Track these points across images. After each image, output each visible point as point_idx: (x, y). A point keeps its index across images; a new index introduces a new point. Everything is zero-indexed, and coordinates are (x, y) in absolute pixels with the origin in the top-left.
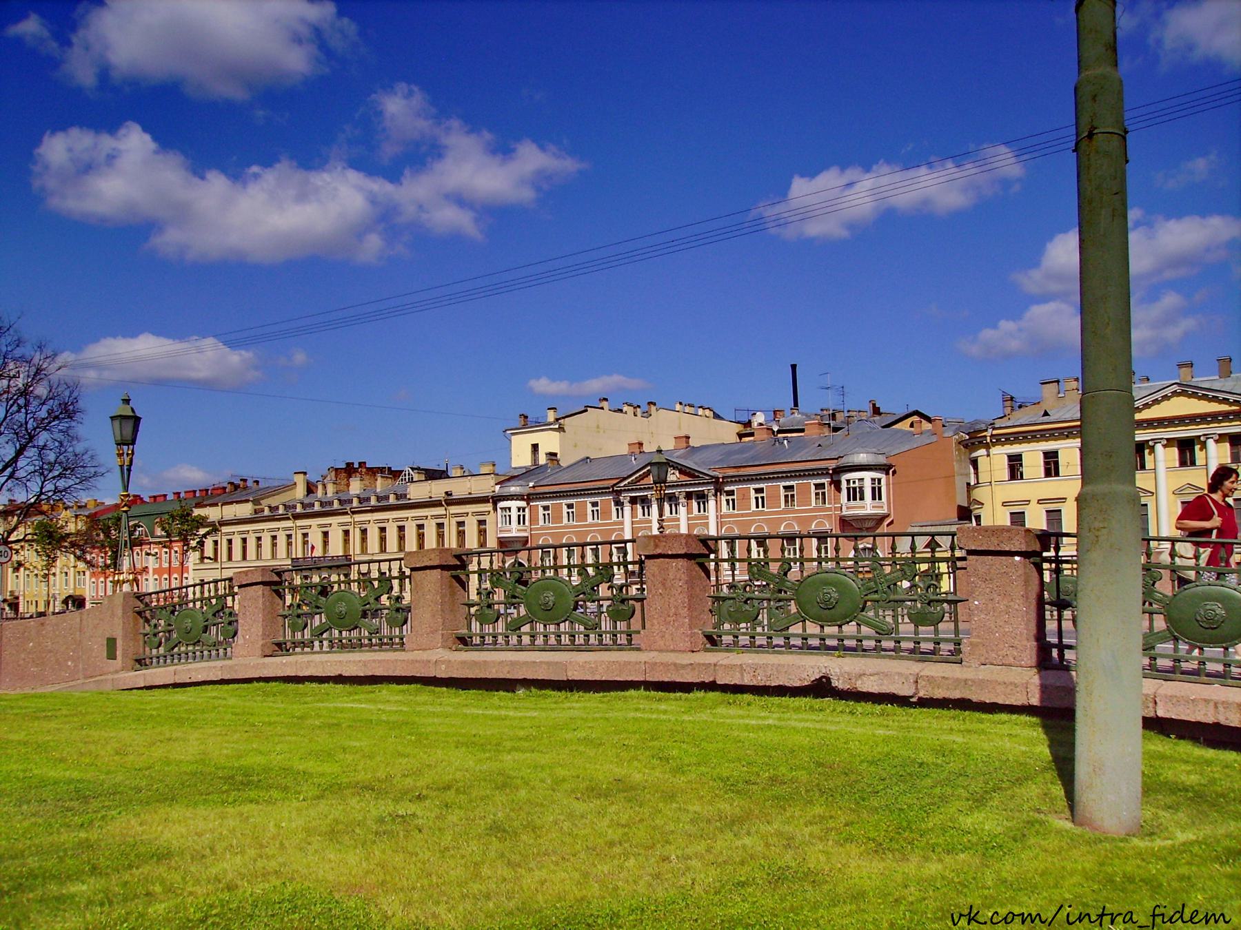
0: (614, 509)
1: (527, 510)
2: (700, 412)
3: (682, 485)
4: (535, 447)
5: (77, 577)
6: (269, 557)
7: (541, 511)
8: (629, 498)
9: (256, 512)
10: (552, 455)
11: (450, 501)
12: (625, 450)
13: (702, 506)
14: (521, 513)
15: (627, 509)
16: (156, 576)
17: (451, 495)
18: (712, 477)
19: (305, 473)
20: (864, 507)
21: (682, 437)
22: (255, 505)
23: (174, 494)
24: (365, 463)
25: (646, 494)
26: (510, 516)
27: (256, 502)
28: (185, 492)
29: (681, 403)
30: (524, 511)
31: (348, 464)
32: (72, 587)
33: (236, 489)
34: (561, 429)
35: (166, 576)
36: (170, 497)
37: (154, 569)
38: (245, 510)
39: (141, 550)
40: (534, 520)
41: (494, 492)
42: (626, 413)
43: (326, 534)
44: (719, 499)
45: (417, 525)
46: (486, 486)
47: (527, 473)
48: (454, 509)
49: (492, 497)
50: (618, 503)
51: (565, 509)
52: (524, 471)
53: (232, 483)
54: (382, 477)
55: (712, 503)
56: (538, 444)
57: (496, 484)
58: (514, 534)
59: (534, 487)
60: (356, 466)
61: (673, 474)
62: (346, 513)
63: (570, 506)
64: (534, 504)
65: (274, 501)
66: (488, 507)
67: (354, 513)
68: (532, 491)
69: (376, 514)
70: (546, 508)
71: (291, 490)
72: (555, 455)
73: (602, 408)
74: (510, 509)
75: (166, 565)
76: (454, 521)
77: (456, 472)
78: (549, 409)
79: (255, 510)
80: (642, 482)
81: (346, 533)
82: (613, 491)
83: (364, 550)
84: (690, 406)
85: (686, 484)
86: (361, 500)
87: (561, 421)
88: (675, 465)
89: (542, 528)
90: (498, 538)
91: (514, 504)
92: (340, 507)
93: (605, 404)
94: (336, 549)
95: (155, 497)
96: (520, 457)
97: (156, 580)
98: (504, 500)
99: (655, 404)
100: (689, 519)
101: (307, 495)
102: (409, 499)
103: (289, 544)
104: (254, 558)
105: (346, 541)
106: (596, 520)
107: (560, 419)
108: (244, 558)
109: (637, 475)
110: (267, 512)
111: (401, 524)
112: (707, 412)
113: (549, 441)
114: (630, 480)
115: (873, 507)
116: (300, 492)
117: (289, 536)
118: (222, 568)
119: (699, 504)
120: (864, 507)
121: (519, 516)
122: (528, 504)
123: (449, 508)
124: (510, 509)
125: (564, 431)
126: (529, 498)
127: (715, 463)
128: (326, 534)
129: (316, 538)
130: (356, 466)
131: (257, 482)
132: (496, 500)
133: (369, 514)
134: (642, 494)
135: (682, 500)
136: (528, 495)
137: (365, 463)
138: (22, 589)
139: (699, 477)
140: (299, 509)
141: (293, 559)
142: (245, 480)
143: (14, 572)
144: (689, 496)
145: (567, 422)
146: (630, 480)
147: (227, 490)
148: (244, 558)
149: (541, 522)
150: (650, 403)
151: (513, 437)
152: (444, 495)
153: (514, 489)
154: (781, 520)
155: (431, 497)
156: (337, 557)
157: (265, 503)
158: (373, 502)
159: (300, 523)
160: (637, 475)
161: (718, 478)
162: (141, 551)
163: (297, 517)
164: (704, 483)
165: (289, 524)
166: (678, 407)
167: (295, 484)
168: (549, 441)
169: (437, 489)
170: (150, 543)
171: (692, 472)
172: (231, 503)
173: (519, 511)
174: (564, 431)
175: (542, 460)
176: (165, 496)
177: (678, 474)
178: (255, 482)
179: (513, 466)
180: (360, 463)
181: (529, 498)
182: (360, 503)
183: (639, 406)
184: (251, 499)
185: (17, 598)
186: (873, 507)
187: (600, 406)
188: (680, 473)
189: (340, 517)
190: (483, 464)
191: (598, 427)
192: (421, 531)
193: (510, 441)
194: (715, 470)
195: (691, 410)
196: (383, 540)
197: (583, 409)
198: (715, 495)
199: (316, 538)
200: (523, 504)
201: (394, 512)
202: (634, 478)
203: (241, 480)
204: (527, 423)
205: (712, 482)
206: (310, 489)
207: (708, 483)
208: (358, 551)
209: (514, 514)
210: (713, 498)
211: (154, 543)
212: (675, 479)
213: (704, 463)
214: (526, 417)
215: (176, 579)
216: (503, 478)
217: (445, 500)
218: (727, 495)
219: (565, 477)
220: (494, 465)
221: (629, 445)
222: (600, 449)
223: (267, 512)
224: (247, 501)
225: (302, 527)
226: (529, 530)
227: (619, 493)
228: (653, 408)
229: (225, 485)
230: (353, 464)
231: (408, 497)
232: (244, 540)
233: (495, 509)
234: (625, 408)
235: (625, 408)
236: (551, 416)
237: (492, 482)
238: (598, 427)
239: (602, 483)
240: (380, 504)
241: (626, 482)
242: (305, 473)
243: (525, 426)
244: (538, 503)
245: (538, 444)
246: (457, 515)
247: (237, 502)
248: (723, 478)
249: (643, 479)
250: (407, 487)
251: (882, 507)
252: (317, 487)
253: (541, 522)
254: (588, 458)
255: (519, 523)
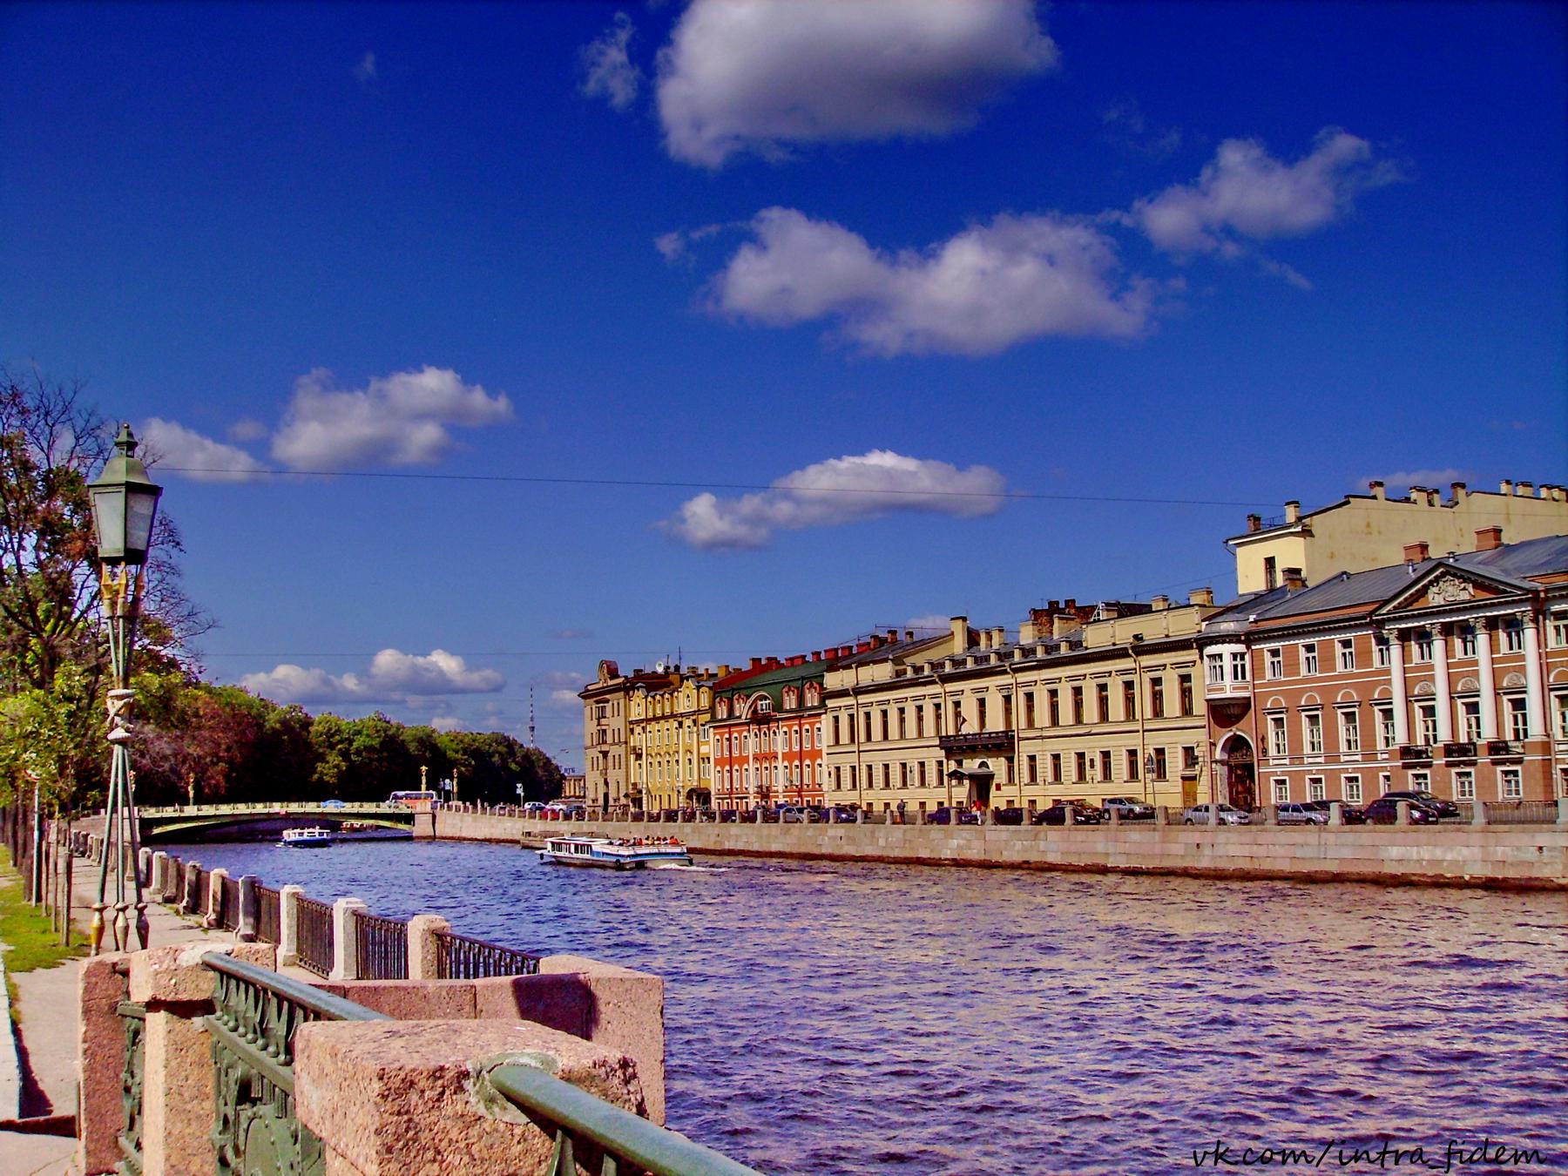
0: (1375, 648)
1: (1247, 657)
2: (1544, 493)
3: (1479, 607)
4: (1270, 562)
5: (702, 765)
6: (915, 736)
7: (1268, 658)
8: (1439, 626)
9: (898, 674)
10: (1293, 573)
11: (1141, 648)
12: (1399, 558)
13: (1469, 645)
14: (1239, 662)
15: (1395, 650)
16: (786, 763)
17: (1141, 639)
18: (1528, 591)
19: (964, 619)
20: (1222, 689)
21: (1488, 531)
22: (896, 665)
23: (813, 654)
24: (1074, 601)
25: (1422, 623)
26: (1221, 667)
27: (898, 661)
28: (825, 651)
29: (1508, 482)
30: (1242, 658)
31: (1051, 603)
32: (696, 777)
33: (882, 645)
34: (1307, 533)
35: (797, 762)
36: (809, 658)
37: (783, 753)
38: (882, 672)
39: (769, 729)
40: (1257, 671)
41: (1199, 632)
42: (1415, 502)
43: (982, 702)
44: (1541, 624)
45: (1180, 676)
46: (1186, 624)
47: (1257, 600)
48: (1147, 660)
49: (1196, 640)
50: (1382, 641)
51: (1303, 653)
52: (1253, 597)
53: (875, 637)
54: (1059, 618)
55: (1529, 634)
56: (1273, 558)
57: (1203, 621)
58: (1228, 695)
59: (1256, 621)
60: (1062, 605)
61: (1464, 589)
62: (1005, 672)
63: (1310, 648)
64: (1258, 647)
65: (919, 659)
66: (1193, 655)
67: (1016, 671)
68: (1253, 628)
69: (1044, 671)
70: (1275, 653)
71: (946, 642)
72: (1298, 571)
73: (1374, 497)
74: (1220, 656)
75: (796, 748)
76: (1147, 677)
77: (1158, 606)
78: (1288, 504)
79: (897, 671)
80: (1416, 606)
81: (1008, 699)
82: (1372, 621)
83: (1030, 723)
84: (1525, 484)
85: (1486, 605)
86: (1001, 656)
87: (1307, 521)
88: (1466, 576)
89: (1270, 684)
90: (1207, 701)
91: (1226, 649)
92: (999, 663)
93: (1379, 491)
94: (995, 724)
95: (792, 659)
96: (1250, 579)
97: (786, 767)
98: (1216, 643)
99: (1463, 486)
100: (1449, 666)
101: (969, 649)
102: (1086, 648)
103: (938, 717)
104: (1071, 720)
105: (1008, 711)
106: (1312, 673)
107: (1305, 517)
108: (886, 737)
109: (1407, 595)
110: (910, 674)
111: (1184, 671)
112: (1556, 493)
113: (1290, 552)
114: (1395, 603)
115: (1234, 689)
116: (958, 645)
117: (938, 706)
118: (859, 752)
119: (1509, 636)
120: (1222, 689)
121: (1235, 667)
122: (1248, 648)
123: (1140, 658)
124: (1220, 656)
125: (1312, 536)
126: (1249, 639)
127: (1536, 567)
128: (982, 702)
129: (970, 709)
130: (1062, 605)
131: (911, 634)
132: (1202, 642)
133: (1035, 672)
134: (1416, 624)
135: (1394, 642)
136: (1247, 634)
137: (1074, 601)
138: (645, 781)
139: (1505, 592)
140: (948, 669)
141: (941, 738)
142: (893, 633)
143: (636, 760)
144: (1404, 636)
145: (1316, 523)
146: (1395, 603)
147: (872, 646)
148: (886, 737)
149: (1269, 675)
150: (1455, 486)
151: (1239, 550)
152: (1131, 640)
153: (1227, 626)
154: (1302, 691)
155: (1114, 644)
156: (997, 733)
157: (908, 660)
158: (1040, 654)
159: (950, 687)
160: (1407, 595)
161: (1537, 592)
162: (760, 731)
163: (946, 679)
164: (1514, 601)
165: (936, 689)
166: (1504, 488)
167: (952, 633)
168: (1290, 552)
169: (1122, 631)
170: (778, 720)
171: (1495, 584)
172: (867, 664)
173: (1235, 659)
174: (1312, 536)
175: (1280, 581)
176: (804, 657)
177: (1471, 590)
178: (908, 633)
179: (1240, 593)
180: (1066, 602)
181: (1249, 639)
182: (1071, 649)
183: (1436, 491)
184: (891, 657)
185: (640, 792)
186: (1234, 689)
187: (1372, 494)
188: (1474, 587)
189: (999, 677)
190: (1194, 591)
191: (1368, 525)
192: (1157, 688)
193: (1234, 555)
194: (1533, 578)
195: (1528, 491)
196: (1054, 708)
197: (1343, 500)
198: (1535, 620)
199: (970, 709)
200: (1240, 648)
201: (1067, 668)
202: (1401, 599)
203: (889, 632)
204: (1260, 527)
205: (1527, 600)
206: (972, 639)
207: (1521, 601)
208: (1023, 724)
209: (1227, 663)
210: (1531, 625)
211: (782, 719)
212: (1467, 597)
213: (1518, 569)
214: (1257, 519)
215: (808, 766)
216: (1213, 611)
217: (1133, 648)
218: (1556, 619)
219: (1313, 602)
220: (1209, 593)
221: (1406, 549)
222: (1373, 560)
223: (910, 674)
224: (886, 660)
225: (953, 693)
226: (1250, 688)
227: (1380, 624)
228: (1461, 493)
229: (868, 640)
230: (1057, 603)
231: (1084, 645)
232: (1054, 693)
233: (1201, 658)
234: (1414, 495)
235: (1414, 495)
236: (1291, 514)
237: (1197, 618)
238: (1368, 525)
239: (1352, 610)
240: (1049, 657)
241: (1390, 607)
242: (964, 619)
243: (1257, 530)
244: (1262, 646)
245: (1273, 558)
246: (1151, 669)
247: (875, 662)
248: (1546, 591)
249: (1417, 600)
250: (1082, 631)
251: (1247, 688)
252: (979, 635)
253: (1269, 675)
254: (1345, 573)
255: (1236, 677)
